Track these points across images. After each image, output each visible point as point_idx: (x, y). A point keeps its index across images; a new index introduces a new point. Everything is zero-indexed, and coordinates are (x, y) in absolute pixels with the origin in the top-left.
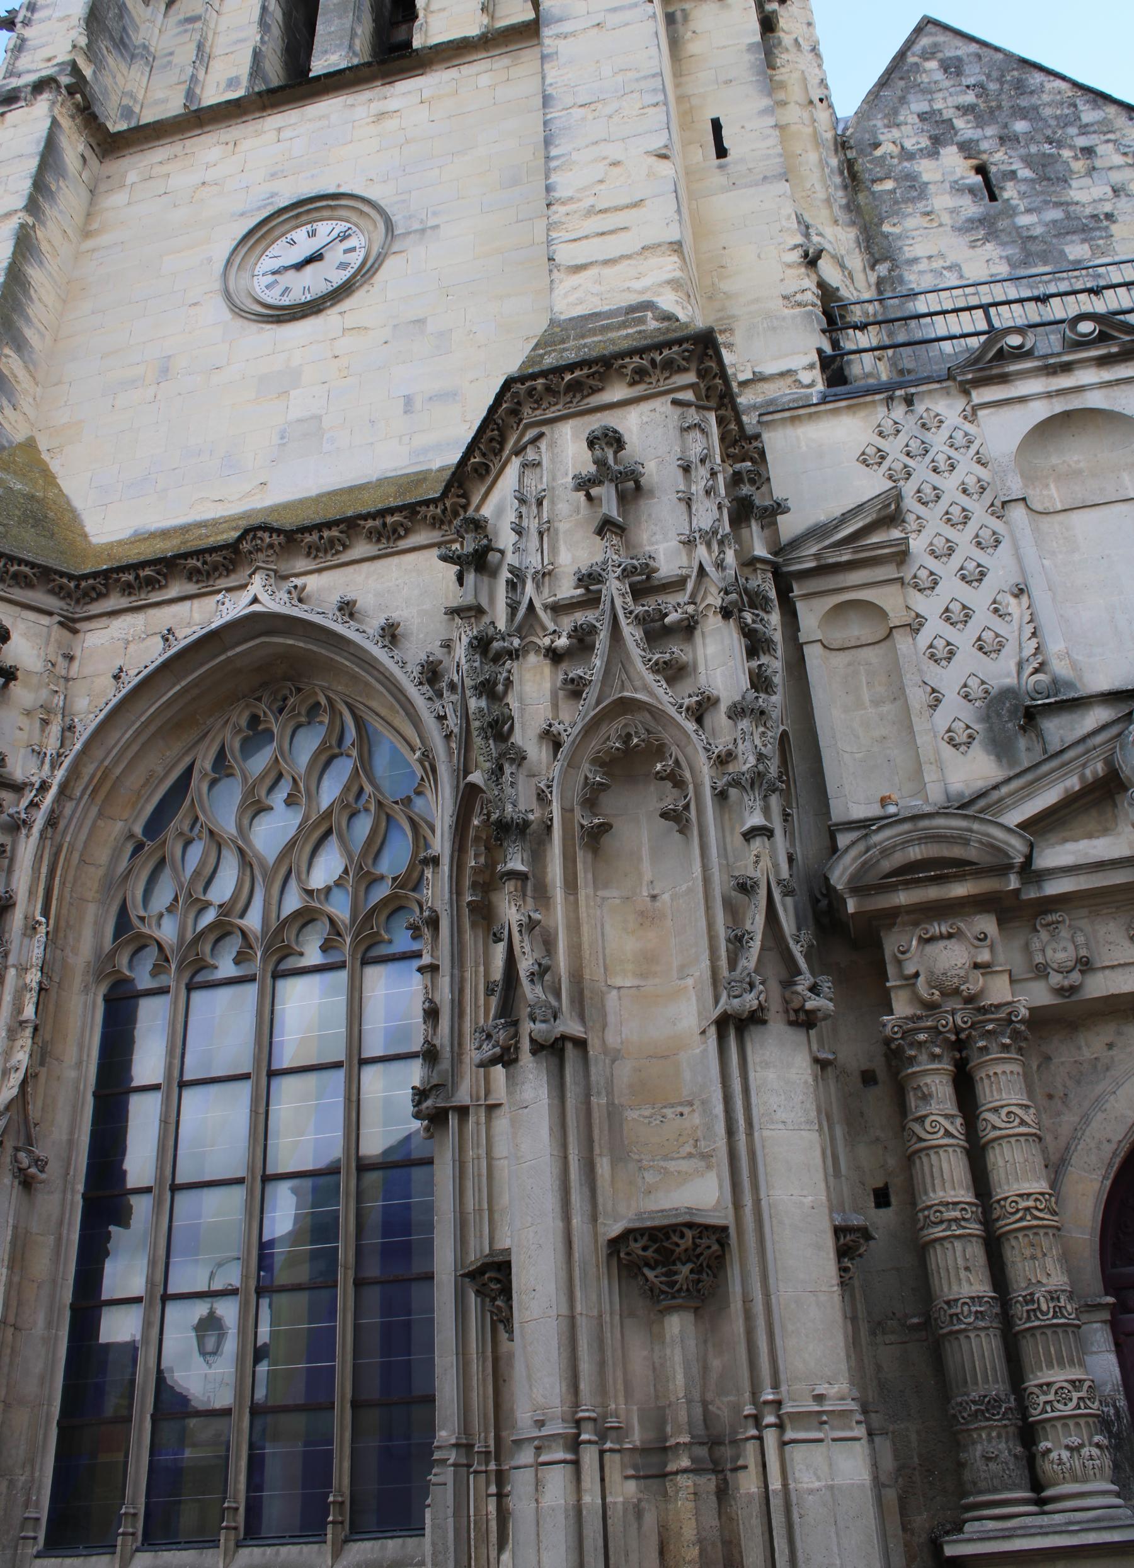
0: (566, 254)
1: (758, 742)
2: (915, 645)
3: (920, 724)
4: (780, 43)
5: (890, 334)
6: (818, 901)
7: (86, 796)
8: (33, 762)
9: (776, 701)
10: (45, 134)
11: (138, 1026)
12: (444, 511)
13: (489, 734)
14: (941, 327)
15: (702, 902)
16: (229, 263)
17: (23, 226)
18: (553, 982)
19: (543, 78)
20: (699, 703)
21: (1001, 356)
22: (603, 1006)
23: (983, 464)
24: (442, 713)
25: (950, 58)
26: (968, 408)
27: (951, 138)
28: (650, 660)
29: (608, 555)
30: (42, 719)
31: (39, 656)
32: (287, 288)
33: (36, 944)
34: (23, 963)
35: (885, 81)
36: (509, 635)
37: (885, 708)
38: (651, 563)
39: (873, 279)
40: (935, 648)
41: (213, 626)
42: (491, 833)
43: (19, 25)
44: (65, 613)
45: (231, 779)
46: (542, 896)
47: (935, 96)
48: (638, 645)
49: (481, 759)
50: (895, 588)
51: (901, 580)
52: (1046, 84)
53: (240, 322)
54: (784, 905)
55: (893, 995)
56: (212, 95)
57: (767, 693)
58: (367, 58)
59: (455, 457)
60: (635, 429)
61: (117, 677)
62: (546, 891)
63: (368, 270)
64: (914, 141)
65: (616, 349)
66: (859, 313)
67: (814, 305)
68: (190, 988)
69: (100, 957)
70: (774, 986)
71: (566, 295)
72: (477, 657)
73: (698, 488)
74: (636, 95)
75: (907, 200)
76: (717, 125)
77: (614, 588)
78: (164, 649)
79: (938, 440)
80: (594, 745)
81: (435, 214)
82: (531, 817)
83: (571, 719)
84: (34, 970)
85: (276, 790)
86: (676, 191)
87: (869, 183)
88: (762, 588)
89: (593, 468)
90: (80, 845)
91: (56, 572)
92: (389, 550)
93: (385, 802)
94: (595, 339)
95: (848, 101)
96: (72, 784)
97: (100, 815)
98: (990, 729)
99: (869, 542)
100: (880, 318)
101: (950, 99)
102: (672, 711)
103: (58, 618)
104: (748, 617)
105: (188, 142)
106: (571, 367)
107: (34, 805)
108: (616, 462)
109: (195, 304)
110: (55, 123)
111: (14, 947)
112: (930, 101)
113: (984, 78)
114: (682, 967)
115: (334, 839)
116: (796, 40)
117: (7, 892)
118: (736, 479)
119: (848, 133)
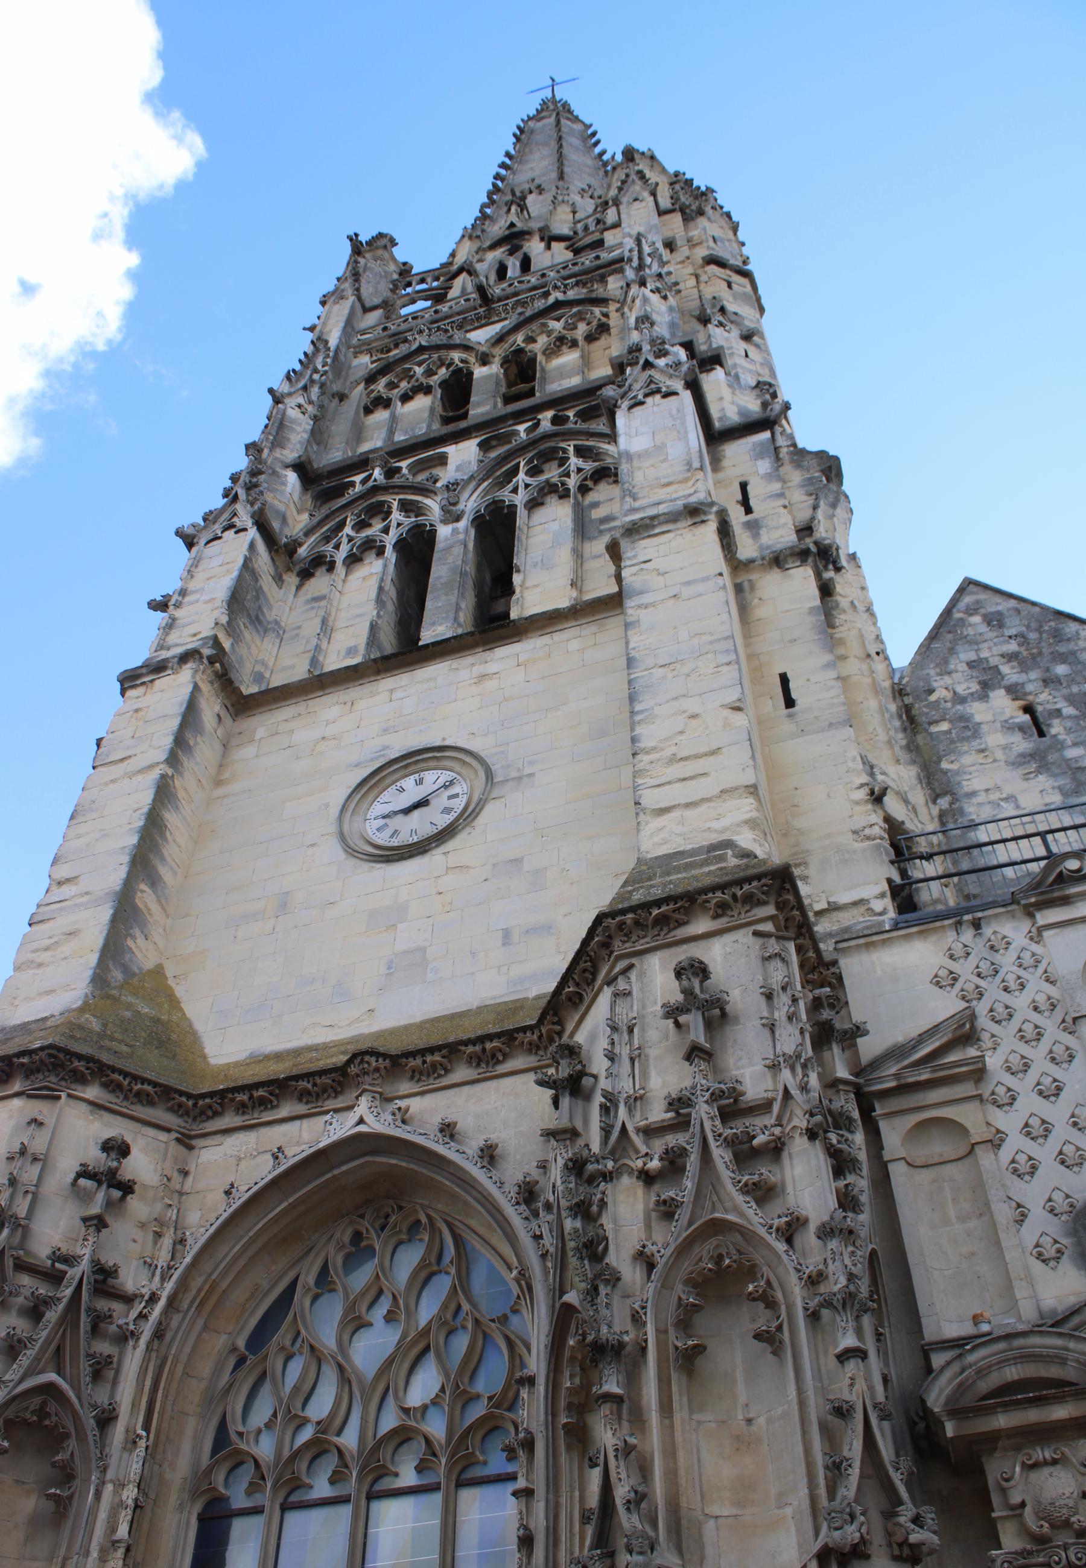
0: (651, 798)
1: (847, 1261)
2: (997, 1160)
3: (1007, 1240)
4: (837, 606)
5: (955, 862)
6: (916, 1424)
7: (193, 1309)
8: (145, 1273)
9: (864, 1219)
10: (187, 697)
11: (230, 1547)
12: (540, 1037)
13: (584, 1254)
14: (1002, 853)
15: (798, 1426)
16: (344, 808)
17: (163, 777)
18: (650, 1511)
19: (627, 643)
20: (788, 1224)
21: (1061, 879)
22: (701, 1537)
23: (1051, 983)
24: (538, 1233)
25: (992, 613)
26: (1034, 930)
27: (999, 683)
28: (739, 1182)
29: (696, 1080)
30: (155, 1232)
31: (155, 1171)
32: (396, 831)
33: (135, 1459)
34: (121, 1478)
35: (934, 635)
36: (603, 1158)
37: (972, 1224)
38: (738, 1087)
39: (935, 811)
40: (1017, 1163)
41: (321, 1145)
42: (586, 1354)
43: (171, 608)
44: (182, 1130)
45: (333, 1294)
46: (638, 1419)
47: (981, 646)
48: (727, 1167)
49: (577, 1279)
50: (974, 1105)
51: (980, 1097)
52: (1081, 632)
53: (352, 862)
54: (881, 1430)
55: (999, 1527)
56: (333, 662)
57: (854, 1212)
58: (470, 629)
59: (551, 986)
60: (719, 959)
61: (228, 1193)
62: (641, 1415)
63: (470, 814)
64: (964, 686)
65: (700, 885)
66: (924, 844)
67: (882, 838)
68: (285, 1508)
69: (196, 1473)
70: (875, 1517)
71: (651, 836)
72: (572, 1178)
73: (780, 1014)
74: (710, 656)
75: (962, 740)
76: (784, 680)
77: (703, 1112)
78: (274, 1167)
79: (1007, 960)
80: (687, 1266)
81: (531, 763)
82: (626, 1338)
83: (664, 1240)
84: (131, 1486)
85: (376, 1306)
86: (750, 740)
87: (926, 726)
88: (845, 1109)
89: (680, 997)
90: (184, 1358)
91: (176, 1091)
92: (488, 1074)
93: (482, 1320)
94: (680, 876)
95: (902, 652)
96: (180, 1296)
97: (206, 1328)
98: (1079, 1243)
99: (946, 1061)
100: (944, 848)
101: (995, 649)
102: (762, 1232)
103: (175, 1135)
104: (833, 1138)
105: (311, 703)
106: (658, 903)
107: (143, 1316)
108: (702, 991)
109: (312, 845)
110: (196, 687)
111: (113, 1462)
112: (976, 651)
113: (1024, 629)
114: (780, 1495)
115: (431, 1355)
116: (852, 602)
117: (110, 1404)
118: (816, 1005)
119: (904, 682)
